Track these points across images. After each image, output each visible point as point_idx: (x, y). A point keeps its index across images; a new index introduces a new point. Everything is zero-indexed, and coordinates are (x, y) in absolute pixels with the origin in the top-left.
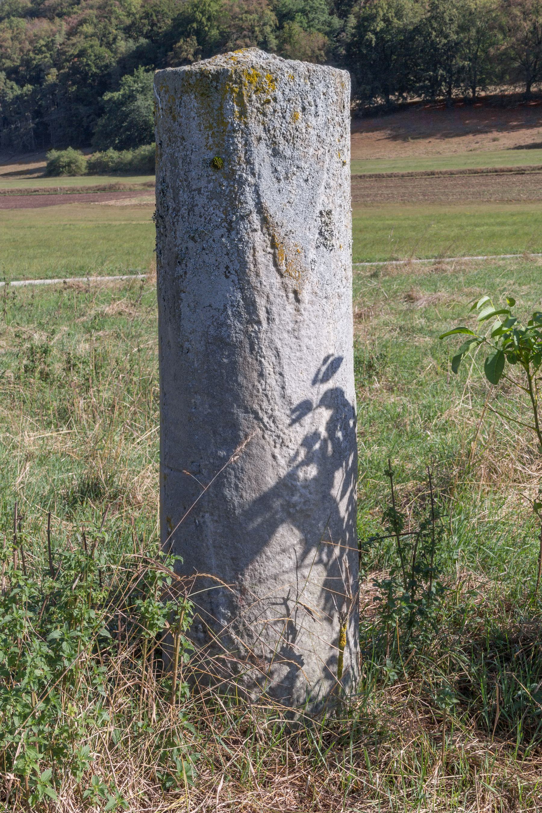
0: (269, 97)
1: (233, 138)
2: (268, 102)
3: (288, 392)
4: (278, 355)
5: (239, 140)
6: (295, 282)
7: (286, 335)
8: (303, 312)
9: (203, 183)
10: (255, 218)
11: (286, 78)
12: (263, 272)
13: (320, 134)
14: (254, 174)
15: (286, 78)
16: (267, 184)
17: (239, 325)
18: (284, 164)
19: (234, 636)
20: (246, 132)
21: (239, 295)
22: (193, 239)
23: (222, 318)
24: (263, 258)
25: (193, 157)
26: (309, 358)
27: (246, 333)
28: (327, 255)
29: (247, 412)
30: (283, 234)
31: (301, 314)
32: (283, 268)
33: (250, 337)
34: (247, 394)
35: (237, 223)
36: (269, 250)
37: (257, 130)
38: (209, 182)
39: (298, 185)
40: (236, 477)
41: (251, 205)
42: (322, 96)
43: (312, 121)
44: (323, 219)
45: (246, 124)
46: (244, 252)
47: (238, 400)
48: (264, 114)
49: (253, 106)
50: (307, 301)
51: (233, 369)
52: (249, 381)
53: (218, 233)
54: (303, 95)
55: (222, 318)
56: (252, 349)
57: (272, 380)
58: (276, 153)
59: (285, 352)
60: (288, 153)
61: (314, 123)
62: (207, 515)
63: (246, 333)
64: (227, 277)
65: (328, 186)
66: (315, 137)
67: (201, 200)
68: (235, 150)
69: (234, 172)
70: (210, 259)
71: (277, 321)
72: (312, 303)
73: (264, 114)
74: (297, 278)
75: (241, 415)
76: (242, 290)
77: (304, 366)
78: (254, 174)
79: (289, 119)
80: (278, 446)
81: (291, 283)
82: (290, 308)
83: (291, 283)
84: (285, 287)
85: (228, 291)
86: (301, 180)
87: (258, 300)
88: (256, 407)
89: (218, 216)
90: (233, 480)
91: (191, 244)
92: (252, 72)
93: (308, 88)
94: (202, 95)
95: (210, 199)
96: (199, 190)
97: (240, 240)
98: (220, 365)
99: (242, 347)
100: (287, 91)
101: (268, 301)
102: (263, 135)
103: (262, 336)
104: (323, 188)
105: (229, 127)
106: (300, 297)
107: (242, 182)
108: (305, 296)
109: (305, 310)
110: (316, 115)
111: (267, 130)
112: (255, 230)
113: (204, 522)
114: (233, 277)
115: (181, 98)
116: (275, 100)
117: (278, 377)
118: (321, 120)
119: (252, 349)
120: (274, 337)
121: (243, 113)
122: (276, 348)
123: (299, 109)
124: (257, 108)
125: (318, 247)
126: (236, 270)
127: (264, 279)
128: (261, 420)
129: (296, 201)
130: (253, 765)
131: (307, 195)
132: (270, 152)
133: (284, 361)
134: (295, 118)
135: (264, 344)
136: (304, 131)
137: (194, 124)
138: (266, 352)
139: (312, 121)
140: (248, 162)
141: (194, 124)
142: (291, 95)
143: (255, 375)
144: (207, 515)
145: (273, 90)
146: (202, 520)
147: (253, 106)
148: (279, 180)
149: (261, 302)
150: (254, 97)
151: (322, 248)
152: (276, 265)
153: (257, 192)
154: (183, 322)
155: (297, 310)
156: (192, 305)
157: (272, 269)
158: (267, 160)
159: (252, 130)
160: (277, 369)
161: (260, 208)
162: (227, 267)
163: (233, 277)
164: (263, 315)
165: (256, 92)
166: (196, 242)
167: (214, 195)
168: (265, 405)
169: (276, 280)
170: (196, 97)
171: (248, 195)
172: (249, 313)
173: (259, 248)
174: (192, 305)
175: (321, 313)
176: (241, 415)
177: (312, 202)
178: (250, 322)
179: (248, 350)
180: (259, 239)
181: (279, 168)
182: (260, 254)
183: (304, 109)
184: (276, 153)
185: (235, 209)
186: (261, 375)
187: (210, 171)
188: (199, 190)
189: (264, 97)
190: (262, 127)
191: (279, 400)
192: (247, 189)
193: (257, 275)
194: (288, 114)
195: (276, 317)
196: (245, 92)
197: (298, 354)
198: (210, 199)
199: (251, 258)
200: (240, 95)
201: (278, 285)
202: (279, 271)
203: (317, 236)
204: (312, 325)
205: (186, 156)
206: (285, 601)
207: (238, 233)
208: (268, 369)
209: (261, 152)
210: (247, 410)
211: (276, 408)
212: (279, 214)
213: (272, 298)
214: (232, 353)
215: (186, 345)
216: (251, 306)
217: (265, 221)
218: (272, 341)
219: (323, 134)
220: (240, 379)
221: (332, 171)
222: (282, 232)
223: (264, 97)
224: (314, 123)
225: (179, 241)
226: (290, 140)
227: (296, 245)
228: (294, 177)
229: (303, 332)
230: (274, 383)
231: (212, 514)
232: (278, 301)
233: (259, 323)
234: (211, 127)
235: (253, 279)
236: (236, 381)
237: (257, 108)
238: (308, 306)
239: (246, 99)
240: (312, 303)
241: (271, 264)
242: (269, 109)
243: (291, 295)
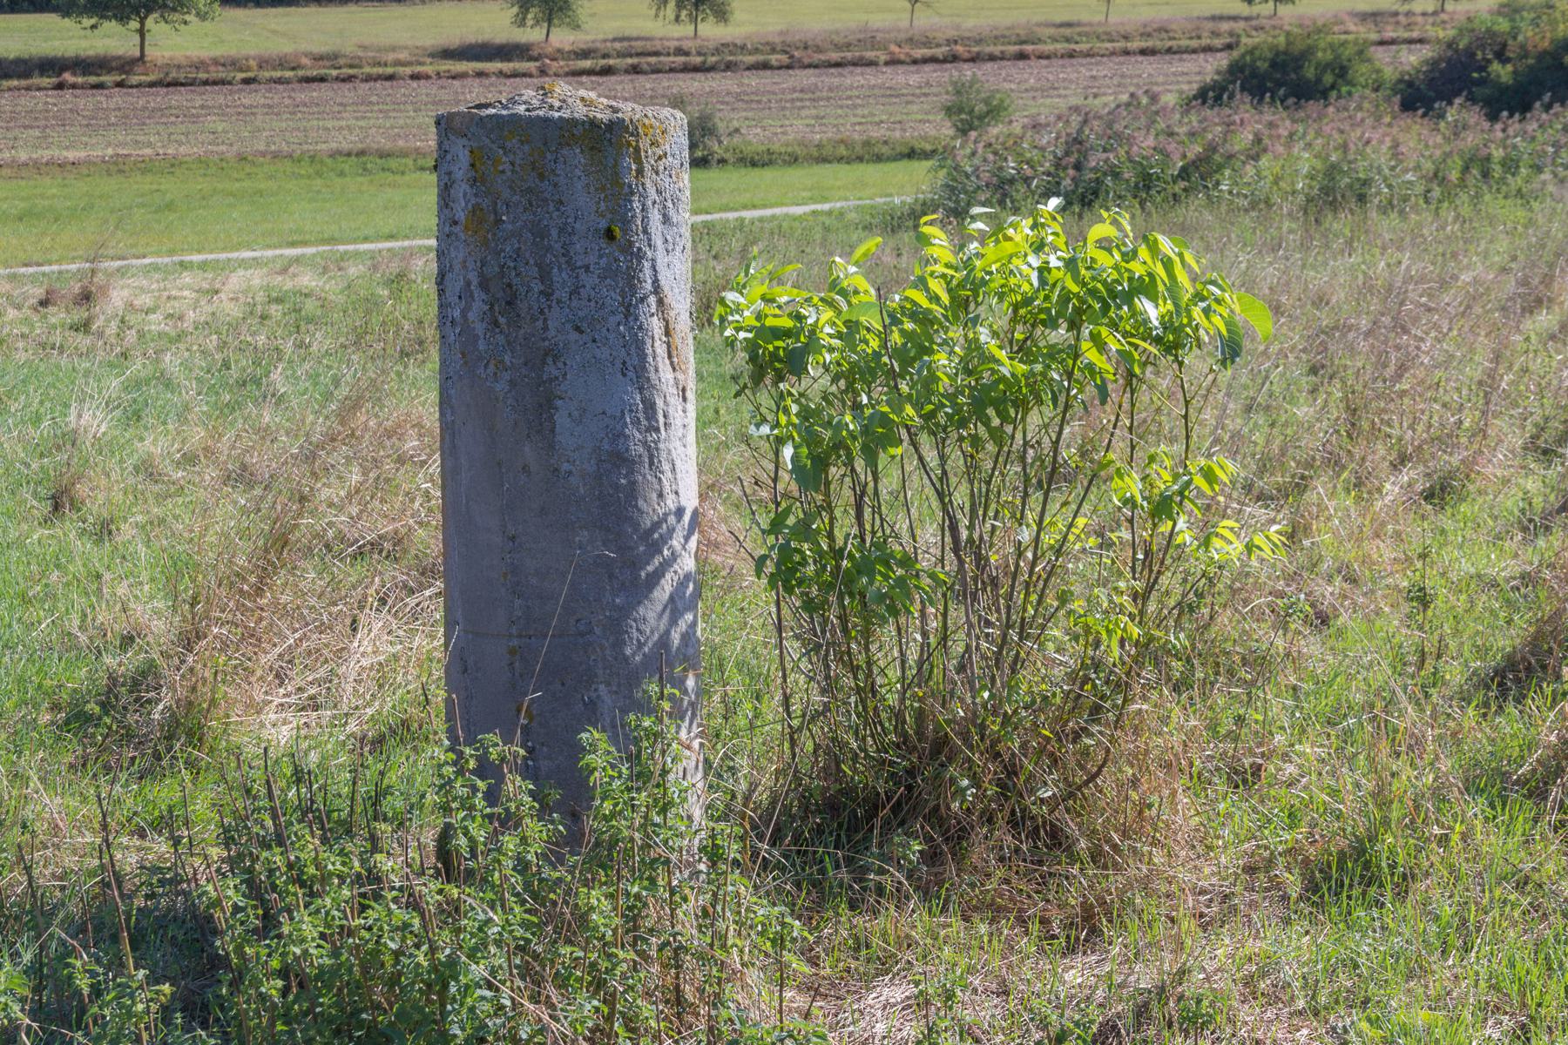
4: (674, 470)
9: (592, 259)
10: (652, 299)
17: (637, 435)
20: (644, 197)
21: (638, 397)
22: (578, 329)
23: (619, 427)
24: (661, 350)
25: (577, 226)
27: (645, 443)
33: (649, 449)
35: (636, 307)
38: (601, 257)
40: (638, 630)
41: (648, 286)
46: (644, 343)
51: (632, 492)
52: (649, 505)
53: (613, 320)
55: (619, 427)
56: (651, 464)
62: (602, 687)
63: (645, 443)
64: (624, 375)
67: (589, 280)
69: (631, 244)
70: (603, 353)
76: (641, 389)
85: (626, 392)
89: (613, 298)
90: (635, 634)
91: (574, 336)
94: (592, 149)
95: (603, 278)
96: (587, 268)
97: (640, 328)
98: (617, 487)
99: (641, 463)
103: (661, 446)
105: (626, 189)
107: (640, 255)
113: (598, 697)
114: (631, 374)
115: (556, 151)
119: (651, 464)
121: (640, 172)
130: (900, 883)
135: (664, 455)
137: (579, 185)
138: (666, 467)
140: (645, 232)
141: (579, 185)
143: (654, 496)
144: (602, 687)
146: (594, 695)
149: (660, 403)
152: (670, 357)
153: (654, 268)
154: (558, 438)
156: (576, 413)
162: (624, 363)
163: (631, 374)
166: (582, 332)
167: (609, 273)
170: (582, 151)
172: (648, 419)
174: (576, 413)
178: (648, 430)
180: (656, 325)
186: (661, 495)
187: (603, 243)
188: (587, 268)
193: (657, 370)
198: (603, 278)
200: (637, 150)
202: (672, 363)
205: (566, 224)
207: (636, 319)
209: (655, 217)
214: (631, 472)
215: (565, 466)
216: (650, 407)
217: (660, 302)
220: (641, 503)
222: (672, 314)
225: (552, 333)
231: (608, 684)
233: (657, 430)
234: (603, 189)
235: (652, 375)
236: (636, 506)
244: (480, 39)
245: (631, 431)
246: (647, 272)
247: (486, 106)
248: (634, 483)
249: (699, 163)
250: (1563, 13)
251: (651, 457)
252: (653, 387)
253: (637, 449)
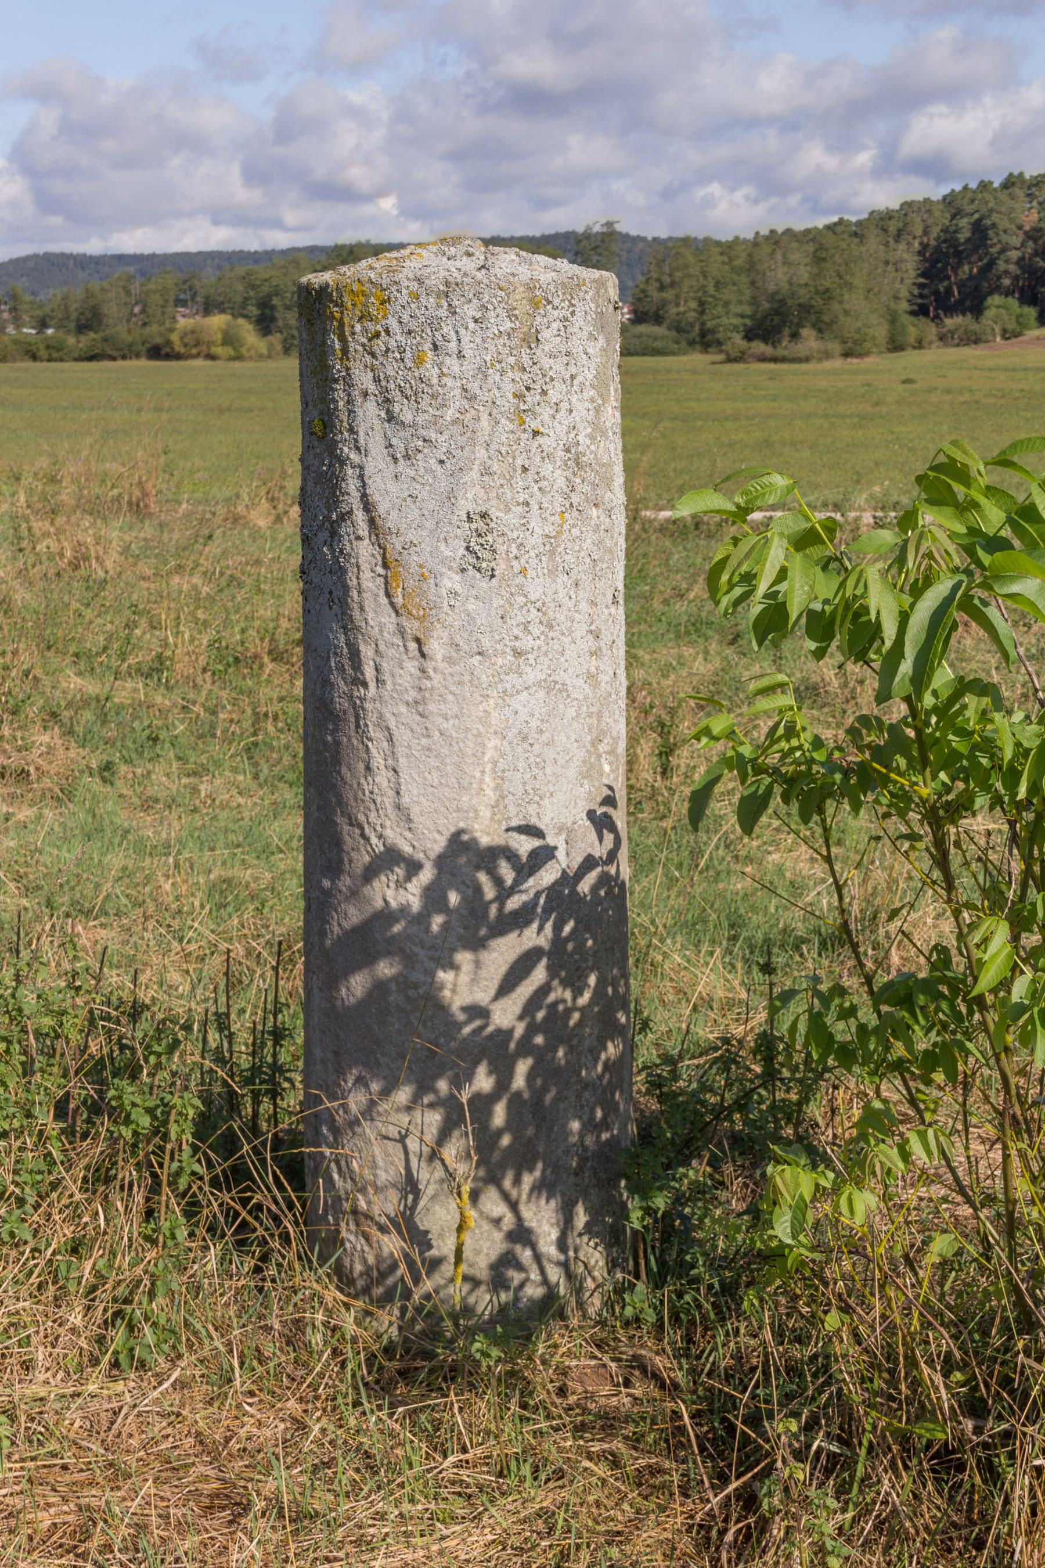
0: (379, 328)
1: (333, 390)
2: (377, 335)
3: (406, 800)
4: (390, 740)
5: (340, 395)
6: (416, 624)
7: (403, 709)
8: (431, 673)
10: (360, 516)
11: (403, 299)
12: (369, 605)
13: (469, 386)
14: (358, 449)
15: (403, 299)
16: (376, 463)
18: (402, 434)
19: (336, 1176)
21: (342, 638)
26: (445, 751)
28: (484, 584)
29: (351, 824)
30: (399, 547)
31: (429, 678)
32: (399, 600)
33: (354, 706)
34: (351, 796)
36: (380, 570)
37: (364, 379)
39: (426, 470)
42: (472, 325)
43: (452, 364)
44: (474, 526)
45: (348, 369)
47: (340, 802)
48: (373, 355)
49: (357, 342)
50: (439, 657)
52: (354, 776)
54: (434, 323)
56: (358, 726)
57: (383, 778)
58: (391, 418)
59: (402, 735)
60: (407, 417)
61: (456, 369)
65: (486, 472)
66: (458, 392)
68: (336, 409)
71: (389, 685)
72: (449, 660)
73: (373, 355)
74: (422, 619)
75: (346, 828)
77: (434, 762)
78: (358, 449)
79: (409, 364)
80: (392, 885)
81: (412, 626)
82: (411, 666)
83: (412, 626)
84: (401, 632)
86: (433, 461)
87: (362, 648)
88: (361, 818)
92: (356, 287)
93: (443, 312)
98: (325, 743)
100: (406, 318)
101: (377, 651)
102: (372, 388)
104: (475, 474)
106: (425, 649)
107: (343, 461)
108: (436, 647)
109: (435, 670)
110: (460, 355)
111: (377, 380)
112: (359, 538)
116: (387, 332)
117: (391, 774)
118: (469, 368)
120: (384, 710)
122: (388, 729)
123: (427, 346)
124: (363, 345)
125: (463, 570)
126: (923, 637)
127: (370, 615)
128: (367, 839)
129: (425, 494)
131: (443, 485)
132: (383, 414)
133: (400, 750)
134: (419, 361)
135: (372, 719)
136: (435, 381)
139: (452, 364)
140: (351, 430)
142: (413, 325)
143: (361, 766)
145: (385, 317)
147: (357, 342)
148: (395, 460)
149: (367, 651)
150: (358, 328)
151: (471, 572)
152: (388, 595)
153: (361, 477)
155: (423, 671)
157: (384, 600)
158: (377, 427)
159: (356, 380)
160: (390, 762)
161: (368, 506)
164: (369, 673)
165: (360, 319)
168: (373, 815)
169: (389, 619)
171: (350, 481)
173: (365, 566)
175: (467, 678)
176: (346, 828)
177: (451, 497)
179: (353, 727)
180: (365, 551)
181: (394, 441)
182: (366, 575)
183: (435, 347)
184: (391, 418)
185: (337, 502)
189: (371, 327)
190: (370, 374)
191: (390, 810)
192: (350, 471)
193: (362, 609)
194: (408, 355)
195: (387, 677)
196: (346, 320)
197: (424, 741)
199: (355, 581)
200: (341, 324)
201: (392, 628)
203: (462, 551)
204: (450, 697)
206: (402, 1139)
208: (378, 761)
209: (369, 413)
210: (354, 823)
211: (388, 823)
212: (394, 515)
213: (382, 647)
217: (372, 522)
218: (381, 717)
219: (474, 387)
220: (344, 770)
221: (494, 447)
222: (397, 543)
223: (371, 327)
224: (456, 369)
226: (412, 396)
227: (421, 566)
228: (420, 456)
229: (432, 707)
230: (385, 784)
232: (391, 652)
233: (365, 685)
235: (356, 614)
237: (363, 345)
238: (441, 665)
239: (347, 330)
240: (449, 660)
241: (382, 593)
242: (379, 346)
243: (413, 646)
244: (238, 248)
245: (335, 677)
246: (352, 485)
247: (343, 340)
248: (337, 743)
249: (305, 316)
250: (1039, 1229)
251: (357, 717)
252: (357, 628)
253: (341, 704)
